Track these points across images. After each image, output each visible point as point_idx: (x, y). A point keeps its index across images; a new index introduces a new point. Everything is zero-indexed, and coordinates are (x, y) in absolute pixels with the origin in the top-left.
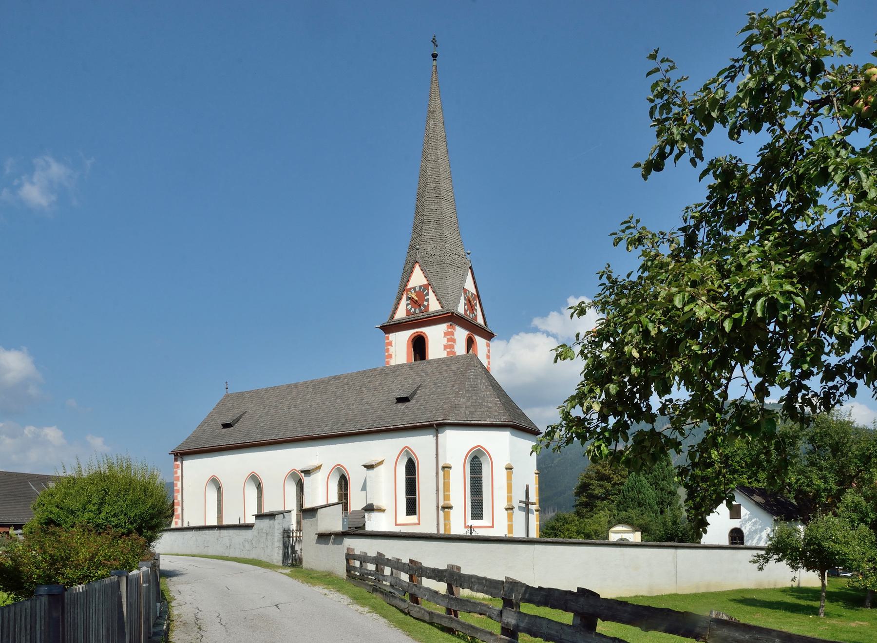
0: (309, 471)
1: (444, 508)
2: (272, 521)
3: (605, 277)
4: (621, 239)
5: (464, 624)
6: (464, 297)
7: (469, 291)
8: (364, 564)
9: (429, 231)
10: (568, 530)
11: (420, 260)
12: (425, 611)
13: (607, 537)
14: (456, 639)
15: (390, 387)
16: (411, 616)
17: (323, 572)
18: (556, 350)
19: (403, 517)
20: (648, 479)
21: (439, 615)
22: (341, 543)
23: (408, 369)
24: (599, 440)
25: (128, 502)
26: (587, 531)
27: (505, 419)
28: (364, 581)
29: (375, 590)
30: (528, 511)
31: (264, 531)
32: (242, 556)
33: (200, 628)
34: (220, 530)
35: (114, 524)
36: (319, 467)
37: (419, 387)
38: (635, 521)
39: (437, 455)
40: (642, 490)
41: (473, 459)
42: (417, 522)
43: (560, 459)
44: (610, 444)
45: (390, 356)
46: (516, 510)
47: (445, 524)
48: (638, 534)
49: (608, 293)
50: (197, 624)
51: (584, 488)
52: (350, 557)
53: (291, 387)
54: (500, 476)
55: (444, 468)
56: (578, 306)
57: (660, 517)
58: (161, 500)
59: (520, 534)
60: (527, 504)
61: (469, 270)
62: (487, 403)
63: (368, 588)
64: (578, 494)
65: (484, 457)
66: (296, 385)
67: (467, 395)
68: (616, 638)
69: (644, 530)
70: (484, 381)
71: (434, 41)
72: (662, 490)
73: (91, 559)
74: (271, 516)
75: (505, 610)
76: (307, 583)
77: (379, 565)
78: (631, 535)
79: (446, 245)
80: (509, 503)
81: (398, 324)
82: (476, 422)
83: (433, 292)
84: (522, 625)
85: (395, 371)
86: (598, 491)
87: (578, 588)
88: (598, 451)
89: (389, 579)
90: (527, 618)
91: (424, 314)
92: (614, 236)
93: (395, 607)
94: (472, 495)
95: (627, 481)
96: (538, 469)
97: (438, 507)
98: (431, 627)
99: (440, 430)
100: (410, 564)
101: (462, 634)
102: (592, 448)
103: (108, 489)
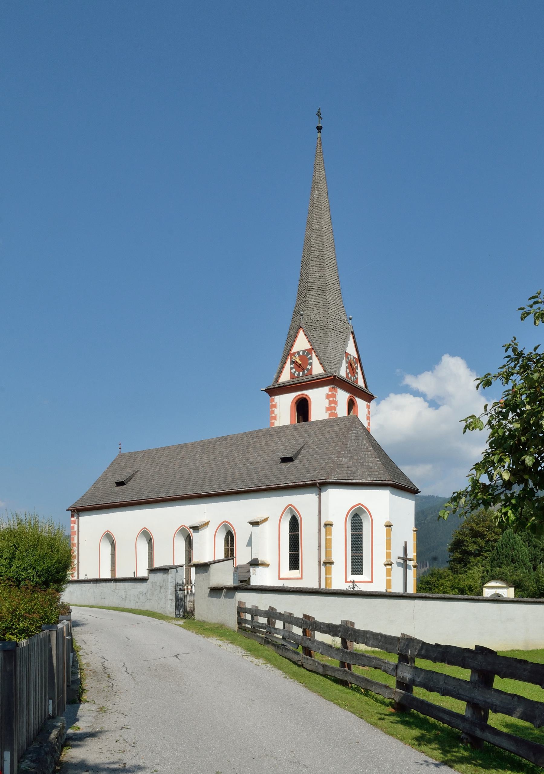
0: (197, 527)
1: (325, 563)
2: (165, 575)
3: (510, 349)
4: (528, 314)
5: (358, 677)
6: (346, 361)
7: (350, 355)
8: (255, 617)
9: (313, 298)
10: (442, 585)
11: (304, 326)
12: (319, 663)
13: (481, 593)
14: (350, 691)
15: (275, 448)
16: (304, 668)
17: (215, 624)
18: (466, 421)
19: (286, 571)
20: (521, 536)
21: (332, 668)
22: (233, 597)
23: (292, 430)
24: (505, 507)
25: (37, 557)
26: (461, 586)
27: (385, 478)
28: (255, 633)
29: (267, 642)
30: (406, 567)
31: (158, 584)
32: (137, 608)
33: (109, 677)
34: (116, 583)
35: (23, 577)
36: (207, 524)
37: (303, 447)
38: (509, 578)
39: (320, 512)
40: (515, 547)
41: (354, 517)
42: (299, 576)
43: (432, 515)
44: (516, 510)
45: (275, 418)
46: (395, 565)
47: (326, 578)
48: (512, 590)
49: (513, 364)
50: (106, 673)
51: (458, 545)
52: (241, 610)
53: (180, 447)
54: (380, 532)
55: (326, 525)
56: (484, 378)
57: (533, 573)
58: (66, 555)
59: (398, 589)
60: (406, 559)
61: (351, 335)
62: (368, 462)
63: (260, 640)
64: (452, 550)
65: (364, 515)
66: (186, 445)
67: (349, 455)
68: (515, 695)
69: (518, 586)
70: (365, 442)
71: (319, 114)
72: (535, 546)
73: (13, 613)
74: (165, 570)
75: (400, 665)
76: (201, 634)
77: (270, 619)
78: (506, 590)
79: (329, 311)
80: (388, 559)
81: (282, 387)
82: (358, 481)
83: (316, 356)
84: (418, 680)
85: (279, 432)
86: (472, 548)
87: (476, 646)
88: (505, 517)
89: (282, 633)
90: (423, 673)
91: (307, 377)
92: (522, 311)
93: (288, 659)
94: (353, 551)
95: (501, 538)
96: (416, 526)
97: (320, 562)
98: (325, 679)
99: (322, 488)
100: (304, 619)
101: (355, 686)
102: (499, 514)
103: (18, 544)
